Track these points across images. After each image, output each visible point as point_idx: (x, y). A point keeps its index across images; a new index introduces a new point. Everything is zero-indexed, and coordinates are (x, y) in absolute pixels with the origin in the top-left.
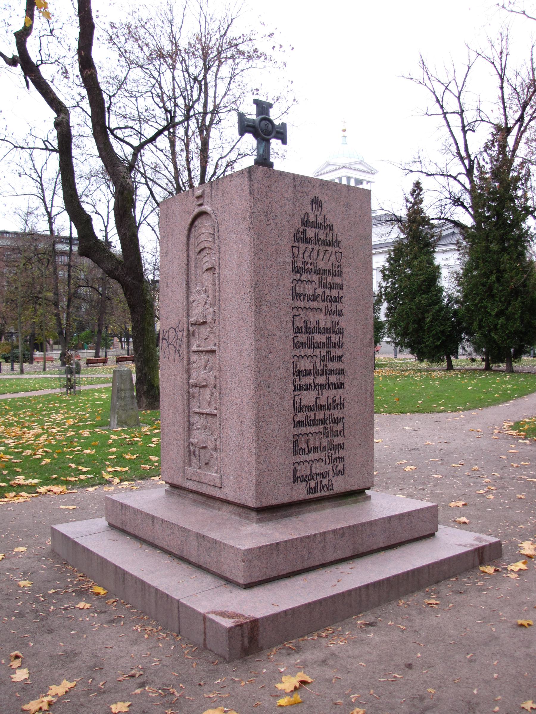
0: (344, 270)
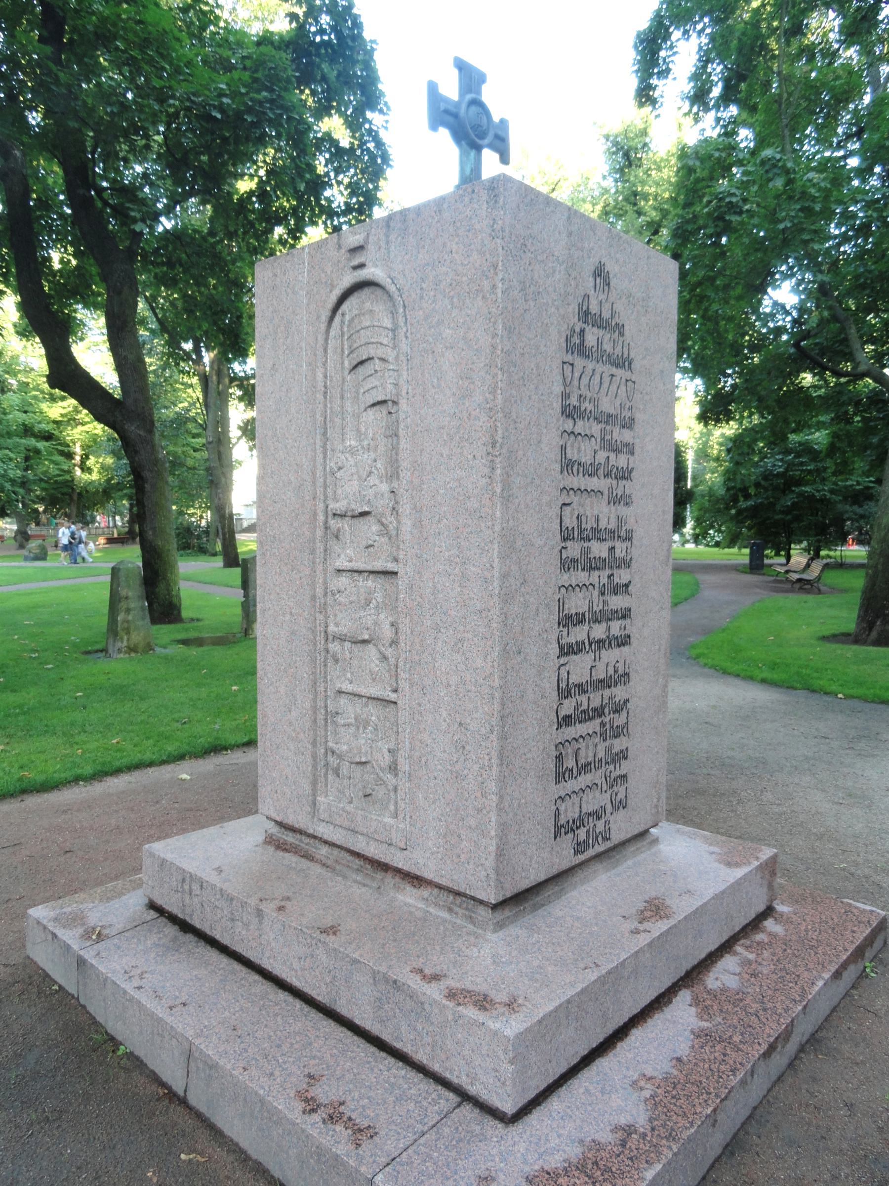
0: (639, 416)
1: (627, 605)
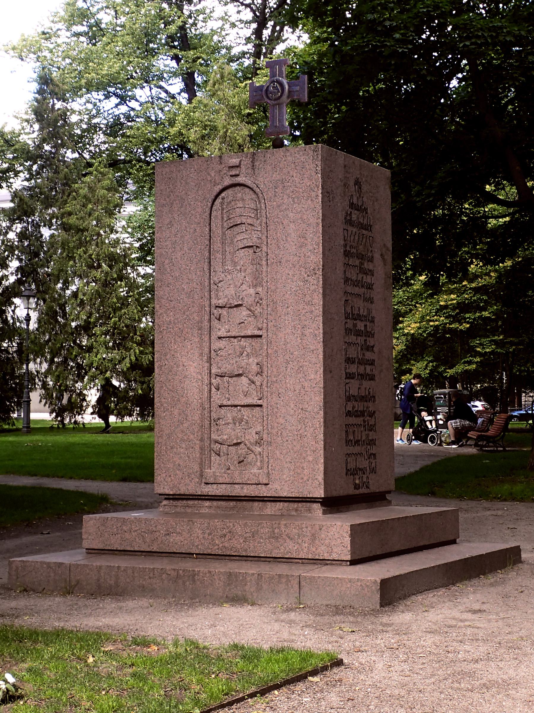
1: (372, 358)
